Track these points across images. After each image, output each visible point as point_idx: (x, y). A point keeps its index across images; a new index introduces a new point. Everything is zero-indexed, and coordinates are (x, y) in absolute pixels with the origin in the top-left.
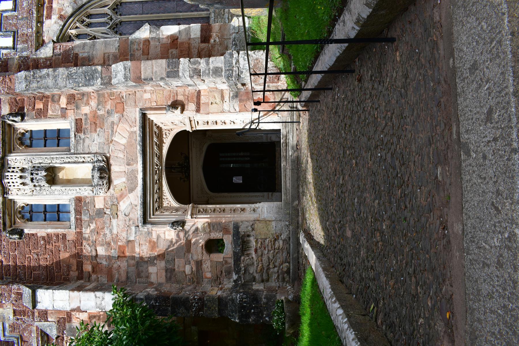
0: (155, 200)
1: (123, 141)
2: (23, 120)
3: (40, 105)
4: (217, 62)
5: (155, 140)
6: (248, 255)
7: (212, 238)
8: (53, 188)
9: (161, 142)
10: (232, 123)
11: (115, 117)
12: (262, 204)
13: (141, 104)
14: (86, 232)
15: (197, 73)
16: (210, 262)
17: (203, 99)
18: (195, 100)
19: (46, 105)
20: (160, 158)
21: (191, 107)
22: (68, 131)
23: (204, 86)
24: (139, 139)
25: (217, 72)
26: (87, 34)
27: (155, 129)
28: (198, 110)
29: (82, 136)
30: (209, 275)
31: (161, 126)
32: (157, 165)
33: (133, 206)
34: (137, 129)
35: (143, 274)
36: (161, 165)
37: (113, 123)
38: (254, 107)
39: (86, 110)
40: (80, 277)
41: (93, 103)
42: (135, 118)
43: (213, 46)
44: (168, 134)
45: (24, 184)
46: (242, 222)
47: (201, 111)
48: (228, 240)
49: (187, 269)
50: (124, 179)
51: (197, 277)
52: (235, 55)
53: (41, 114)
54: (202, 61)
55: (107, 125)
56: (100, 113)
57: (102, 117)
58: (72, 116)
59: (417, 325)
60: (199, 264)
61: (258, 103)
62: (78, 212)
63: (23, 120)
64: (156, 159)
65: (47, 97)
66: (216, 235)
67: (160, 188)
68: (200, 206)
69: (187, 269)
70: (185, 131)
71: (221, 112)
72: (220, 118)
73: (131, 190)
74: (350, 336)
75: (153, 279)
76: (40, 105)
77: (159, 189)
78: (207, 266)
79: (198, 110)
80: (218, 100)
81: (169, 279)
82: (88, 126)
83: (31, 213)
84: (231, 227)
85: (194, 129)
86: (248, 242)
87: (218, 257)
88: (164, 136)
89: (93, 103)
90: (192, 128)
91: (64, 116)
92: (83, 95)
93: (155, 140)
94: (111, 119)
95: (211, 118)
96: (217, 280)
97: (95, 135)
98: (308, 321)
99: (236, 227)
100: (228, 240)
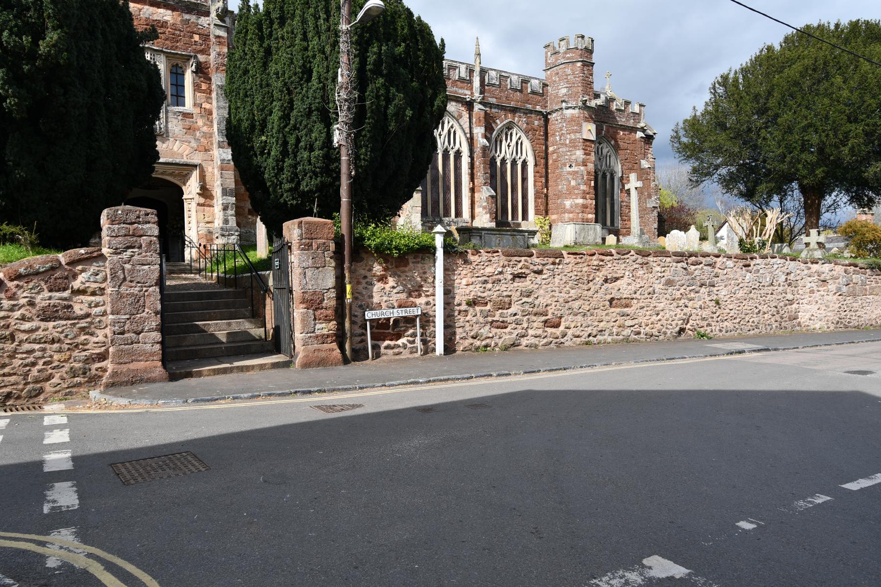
1: (175, 148)
2: (193, 72)
3: (204, 86)
4: (233, 222)
9: (175, 176)
11: (194, 144)
15: (225, 208)
19: (204, 92)
21: (202, 200)
22: (184, 105)
23: (217, 209)
24: (178, 161)
25: (226, 221)
28: (199, 205)
34: (185, 160)
37: (190, 142)
38: (202, 244)
39: (200, 123)
41: (205, 129)
43: (246, 217)
52: (237, 233)
53: (197, 88)
54: (233, 212)
55: (188, 137)
56: (198, 134)
58: (196, 111)
59: (432, 113)
61: (205, 247)
63: (193, 72)
65: (210, 94)
72: (194, 220)
74: (880, 478)
79: (199, 205)
80: (207, 219)
82: (187, 123)
89: (205, 129)
92: (212, 122)
94: (193, 141)
95: (193, 213)
97: (180, 127)
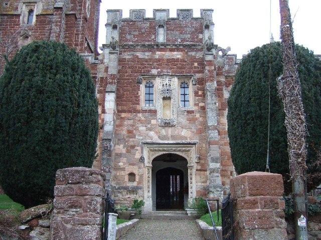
6: (127, 194)
7: (136, 176)
8: (162, 100)
12: (151, 201)
14: (140, 115)
16: (125, 175)
17: (202, 172)
19: (200, 96)
26: (165, 161)
29: (186, 114)
30: (118, 174)
33: (151, 138)
34: (188, 141)
35: (119, 141)
40: (119, 111)
45: (163, 85)
48: (135, 184)
49: (121, 164)
50: (165, 134)
51: (118, 169)
57: (194, 123)
60: (123, 169)
62: (150, 111)
66: (137, 178)
67: (160, 151)
69: (121, 164)
73: (159, 137)
75: (117, 146)
76: (200, 93)
78: (122, 173)
81: (117, 154)
83: (150, 86)
84: (141, 186)
86: (134, 194)
87: (127, 178)
91: (195, 105)
96: (116, 177)
98: (97, 149)
99: (141, 188)
100: (135, 184)
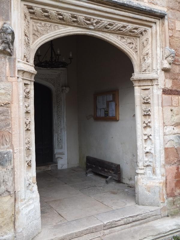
0: (47, 8)
5: (130, 26)
9: (119, 32)
10: (146, 137)
13: (170, 16)
18: (174, 88)
20: (105, 29)
27: (142, 28)
28: (166, 92)
31: (144, 38)
32: (97, 23)
36: (99, 30)
42: (157, 4)
44: (131, 46)
46: (13, 169)
47: (164, 95)
64: (106, 22)
67: (62, 21)
68: (32, 87)
70: (133, 71)
71: (164, 123)
77: (62, 19)
79: (166, 92)
85: (136, 84)
88: (129, 41)
90: (139, 81)
93: (130, 26)
